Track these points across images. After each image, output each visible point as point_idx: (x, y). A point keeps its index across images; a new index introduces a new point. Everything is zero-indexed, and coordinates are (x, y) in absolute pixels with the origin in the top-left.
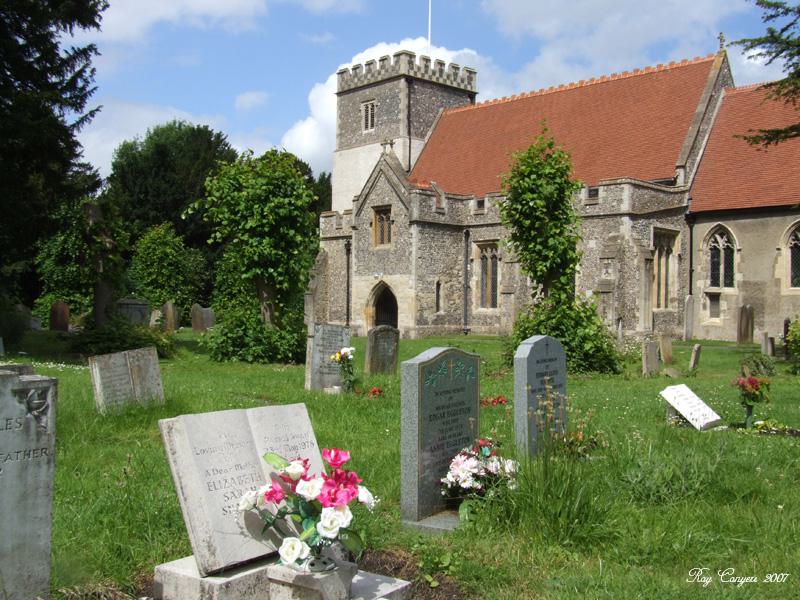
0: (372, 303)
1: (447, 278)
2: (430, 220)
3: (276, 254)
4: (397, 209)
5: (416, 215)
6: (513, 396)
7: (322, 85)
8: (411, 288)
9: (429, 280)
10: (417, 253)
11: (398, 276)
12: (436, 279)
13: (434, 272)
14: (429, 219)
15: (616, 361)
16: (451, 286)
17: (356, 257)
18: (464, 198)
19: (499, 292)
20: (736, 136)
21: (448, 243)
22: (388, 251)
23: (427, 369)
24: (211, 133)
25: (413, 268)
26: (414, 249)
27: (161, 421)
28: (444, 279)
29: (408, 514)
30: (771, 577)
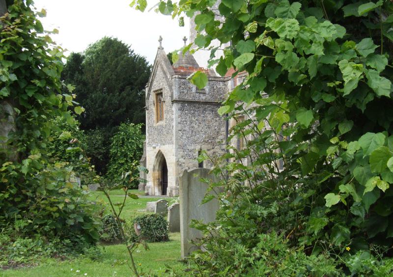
0: (157, 168)
1: (210, 146)
2: (190, 99)
5: (175, 97)
7: (369, 81)
8: (174, 155)
9: (190, 148)
10: (177, 126)
11: (167, 146)
12: (198, 147)
13: (195, 142)
14: (187, 98)
16: (214, 153)
17: (148, 132)
18: (226, 80)
21: (209, 117)
22: (162, 126)
24: (145, 61)
26: (174, 124)
27: (372, 99)
28: (205, 147)
29: (248, 268)
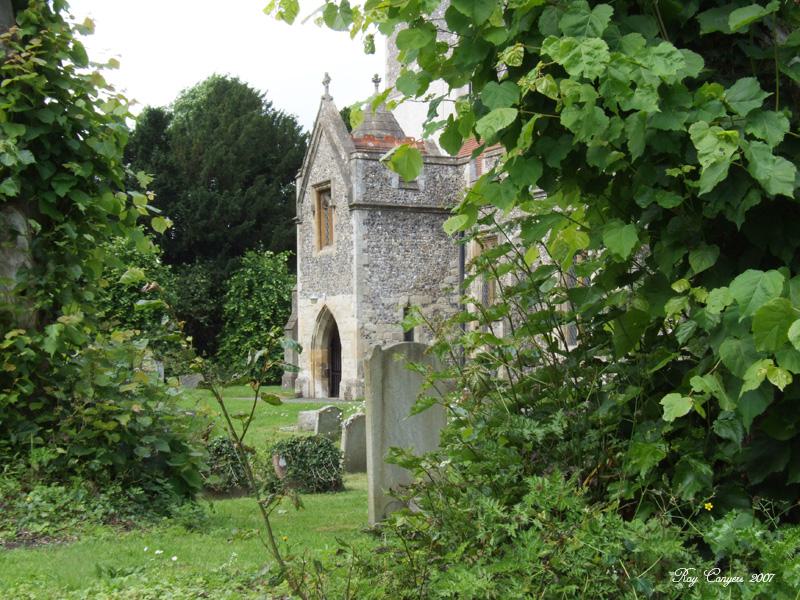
1: (427, 298)
3: (538, 370)
4: (338, 188)
5: (357, 197)
6: (772, 13)
9: (387, 301)
12: (403, 300)
13: (397, 289)
14: (380, 199)
15: (124, 144)
16: (436, 311)
17: (301, 270)
19: (309, 184)
20: (401, 486)
22: (329, 257)
23: (675, 361)
25: (354, 282)
26: (354, 252)
28: (417, 300)
30: (757, 577)
